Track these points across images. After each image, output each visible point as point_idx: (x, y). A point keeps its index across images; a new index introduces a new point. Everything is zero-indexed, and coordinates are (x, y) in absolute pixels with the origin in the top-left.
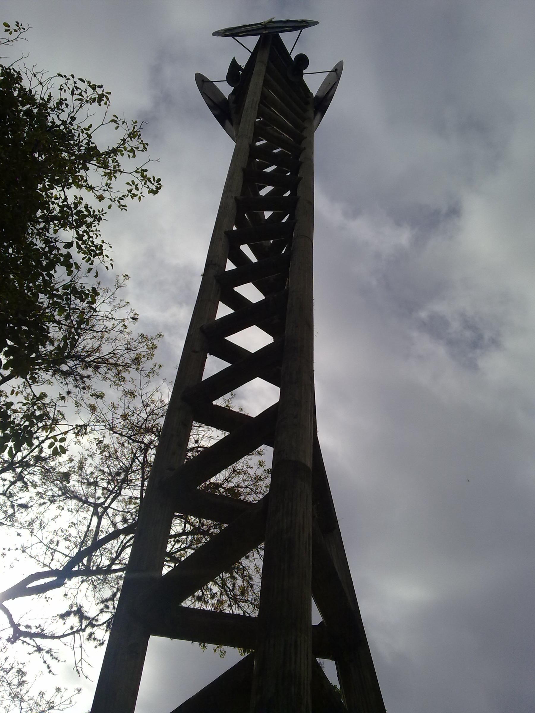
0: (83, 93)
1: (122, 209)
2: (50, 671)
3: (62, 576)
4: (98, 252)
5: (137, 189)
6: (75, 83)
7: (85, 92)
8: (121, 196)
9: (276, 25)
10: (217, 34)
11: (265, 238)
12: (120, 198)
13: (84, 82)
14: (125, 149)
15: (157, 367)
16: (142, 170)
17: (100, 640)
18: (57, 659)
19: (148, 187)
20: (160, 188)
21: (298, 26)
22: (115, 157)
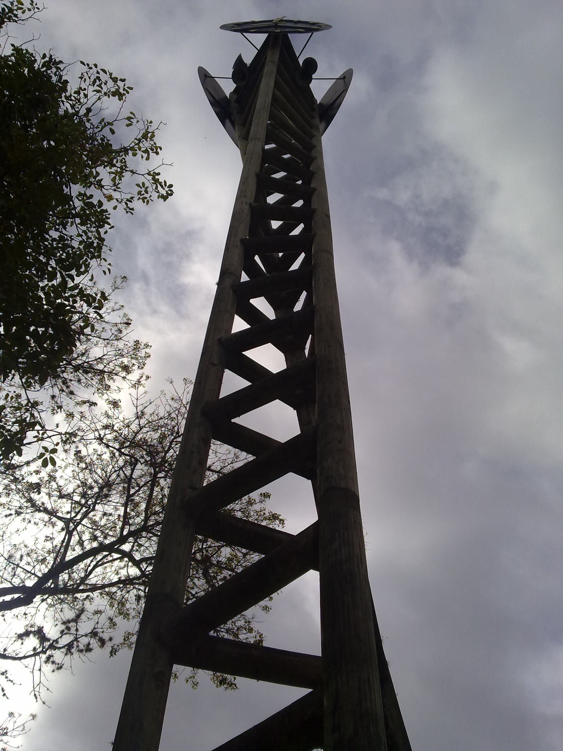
0: (103, 85)
1: (127, 212)
2: (4, 695)
3: (26, 596)
4: (96, 254)
5: (146, 192)
6: (98, 73)
7: (105, 84)
8: (129, 198)
9: (287, 24)
10: (224, 27)
11: (279, 259)
12: (128, 200)
13: (106, 74)
14: (140, 148)
15: (144, 378)
16: (154, 173)
17: (58, 664)
18: (12, 681)
19: (158, 192)
20: (171, 195)
21: (311, 28)
22: (124, 157)
